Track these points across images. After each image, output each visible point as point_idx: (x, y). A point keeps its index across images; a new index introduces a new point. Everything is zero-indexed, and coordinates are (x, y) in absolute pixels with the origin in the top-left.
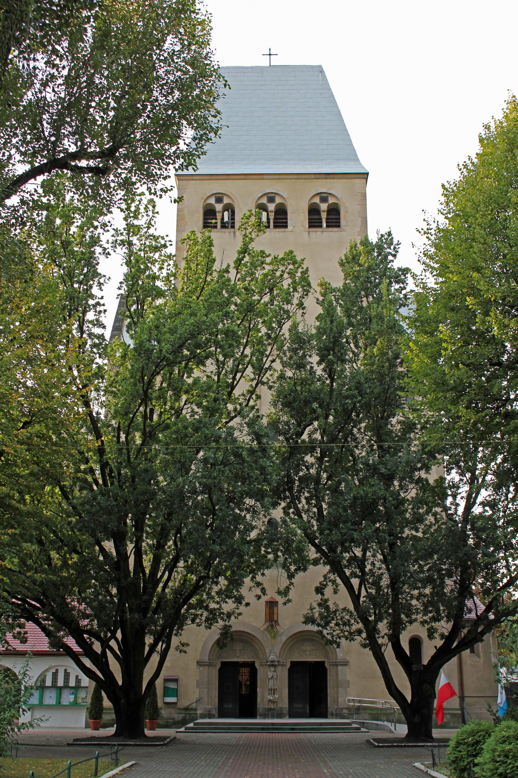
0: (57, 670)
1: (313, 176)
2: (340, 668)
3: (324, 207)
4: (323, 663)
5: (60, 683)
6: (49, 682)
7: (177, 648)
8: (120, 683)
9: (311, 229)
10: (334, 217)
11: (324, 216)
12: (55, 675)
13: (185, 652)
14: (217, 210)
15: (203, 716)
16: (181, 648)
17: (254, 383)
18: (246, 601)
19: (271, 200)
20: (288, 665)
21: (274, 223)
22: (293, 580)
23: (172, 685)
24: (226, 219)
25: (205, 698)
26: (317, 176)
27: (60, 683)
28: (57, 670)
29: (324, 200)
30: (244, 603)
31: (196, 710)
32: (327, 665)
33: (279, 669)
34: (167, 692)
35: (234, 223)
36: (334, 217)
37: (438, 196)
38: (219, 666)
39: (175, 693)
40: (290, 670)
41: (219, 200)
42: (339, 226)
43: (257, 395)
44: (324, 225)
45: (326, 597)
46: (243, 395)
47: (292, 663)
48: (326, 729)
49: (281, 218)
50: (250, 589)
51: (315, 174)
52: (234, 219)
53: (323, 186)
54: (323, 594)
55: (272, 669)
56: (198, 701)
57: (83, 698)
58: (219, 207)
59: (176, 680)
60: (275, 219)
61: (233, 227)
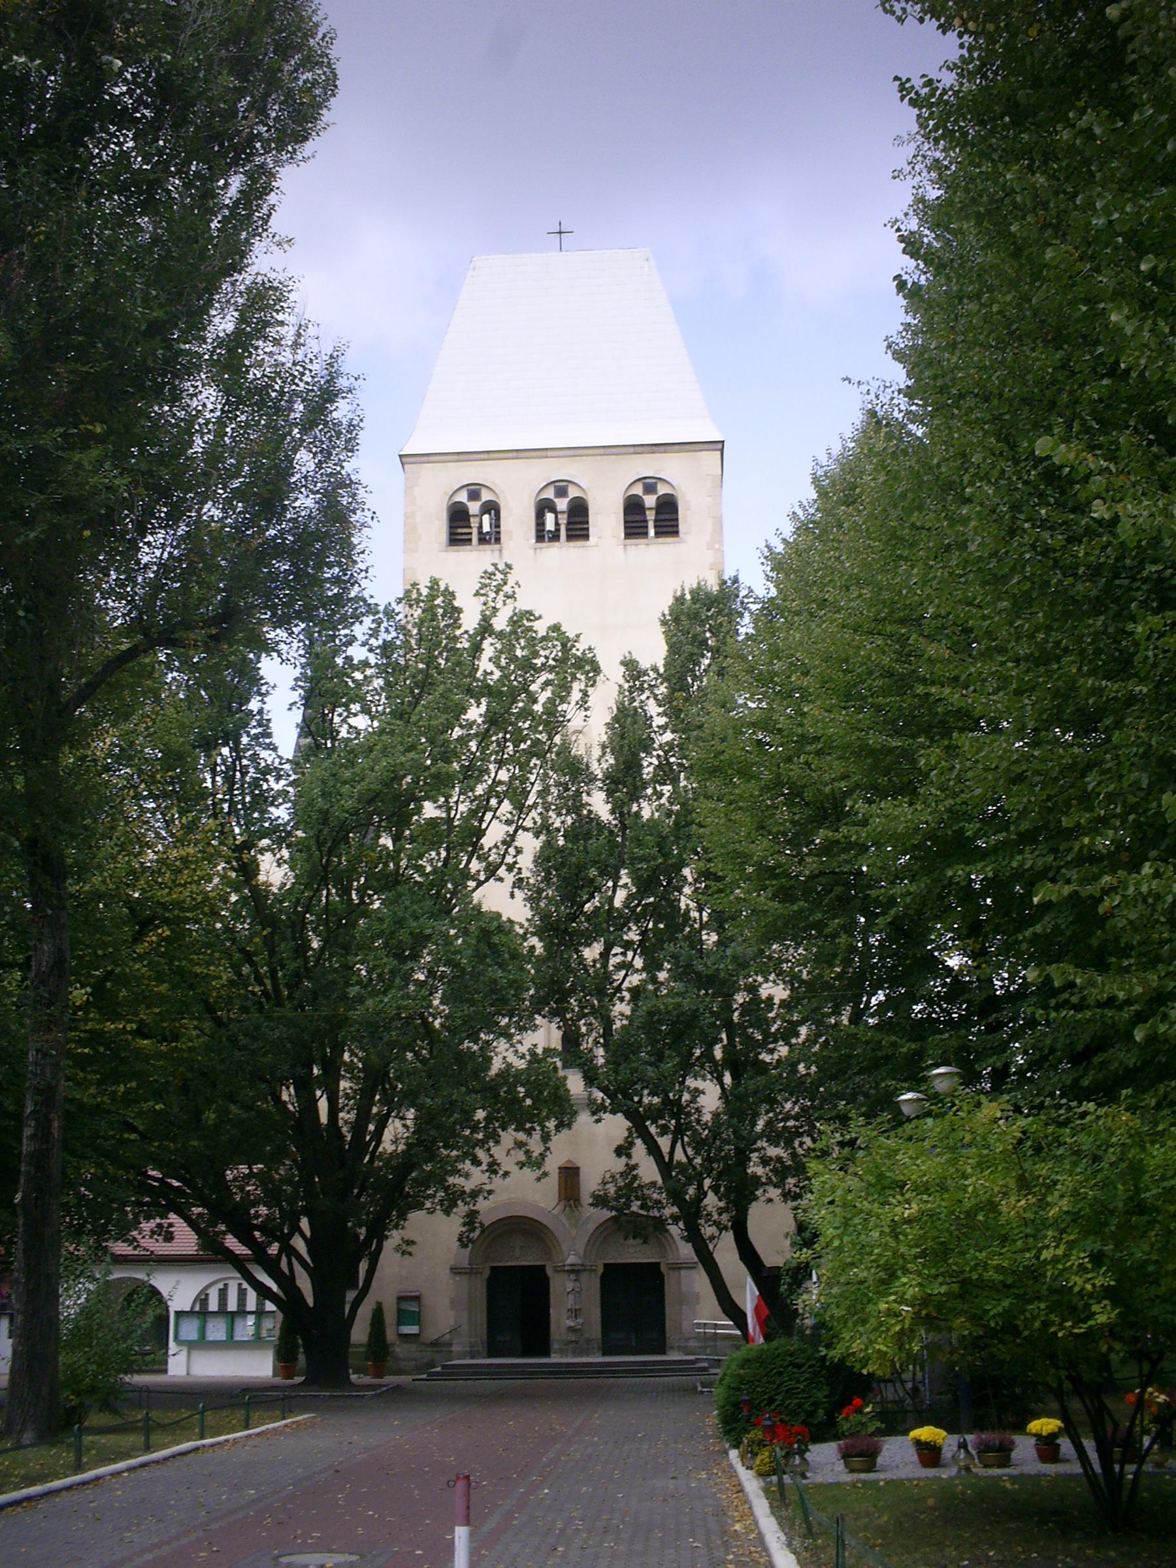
0: (226, 1285)
1: (632, 450)
2: (683, 1272)
3: (650, 501)
4: (542, 1268)
5: (232, 1306)
6: (213, 1305)
7: (397, 1249)
8: (310, 1302)
9: (629, 541)
10: (667, 517)
11: (651, 516)
12: (223, 1294)
13: (410, 1254)
14: (471, 512)
15: (462, 1356)
16: (404, 1247)
17: (511, 829)
18: (504, 1168)
19: (561, 492)
20: (601, 1270)
21: (567, 530)
22: (550, 1144)
23: (412, 1307)
24: (486, 528)
25: (465, 1328)
26: (638, 449)
27: (232, 1306)
28: (226, 1285)
29: (650, 488)
30: (501, 1172)
31: (451, 1345)
32: (663, 1268)
33: (584, 1276)
34: (403, 1317)
35: (499, 533)
36: (667, 517)
37: (604, 729)
38: (487, 1274)
39: (416, 1318)
40: (603, 1278)
41: (474, 495)
42: (675, 533)
43: (516, 847)
44: (652, 532)
45: (632, 1162)
46: (496, 846)
47: (606, 1265)
48: (652, 1371)
49: (578, 522)
50: (508, 1153)
51: (634, 446)
52: (498, 526)
53: (648, 467)
54: (629, 1156)
55: (573, 1277)
56: (453, 1331)
57: (269, 1330)
58: (474, 508)
59: (417, 1298)
60: (568, 523)
61: (498, 540)
